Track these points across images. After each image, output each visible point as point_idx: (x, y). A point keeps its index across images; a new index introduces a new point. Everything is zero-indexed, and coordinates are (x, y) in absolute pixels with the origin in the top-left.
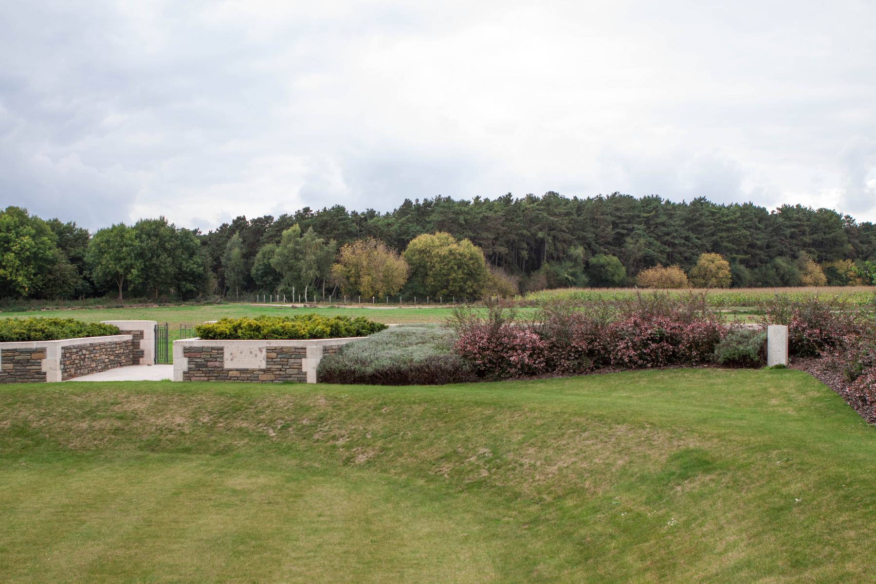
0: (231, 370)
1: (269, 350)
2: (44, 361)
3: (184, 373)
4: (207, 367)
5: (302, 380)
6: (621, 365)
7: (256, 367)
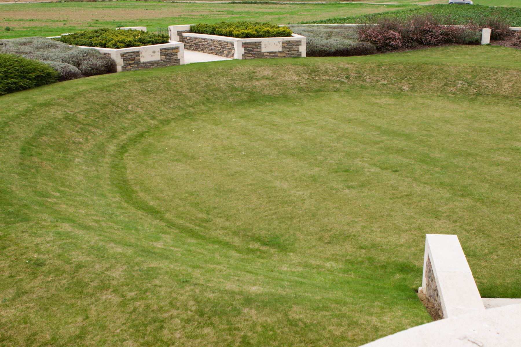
0: (265, 53)
1: (283, 42)
2: (179, 54)
3: (243, 55)
4: (253, 51)
5: (299, 56)
6: (429, 44)
7: (277, 50)
